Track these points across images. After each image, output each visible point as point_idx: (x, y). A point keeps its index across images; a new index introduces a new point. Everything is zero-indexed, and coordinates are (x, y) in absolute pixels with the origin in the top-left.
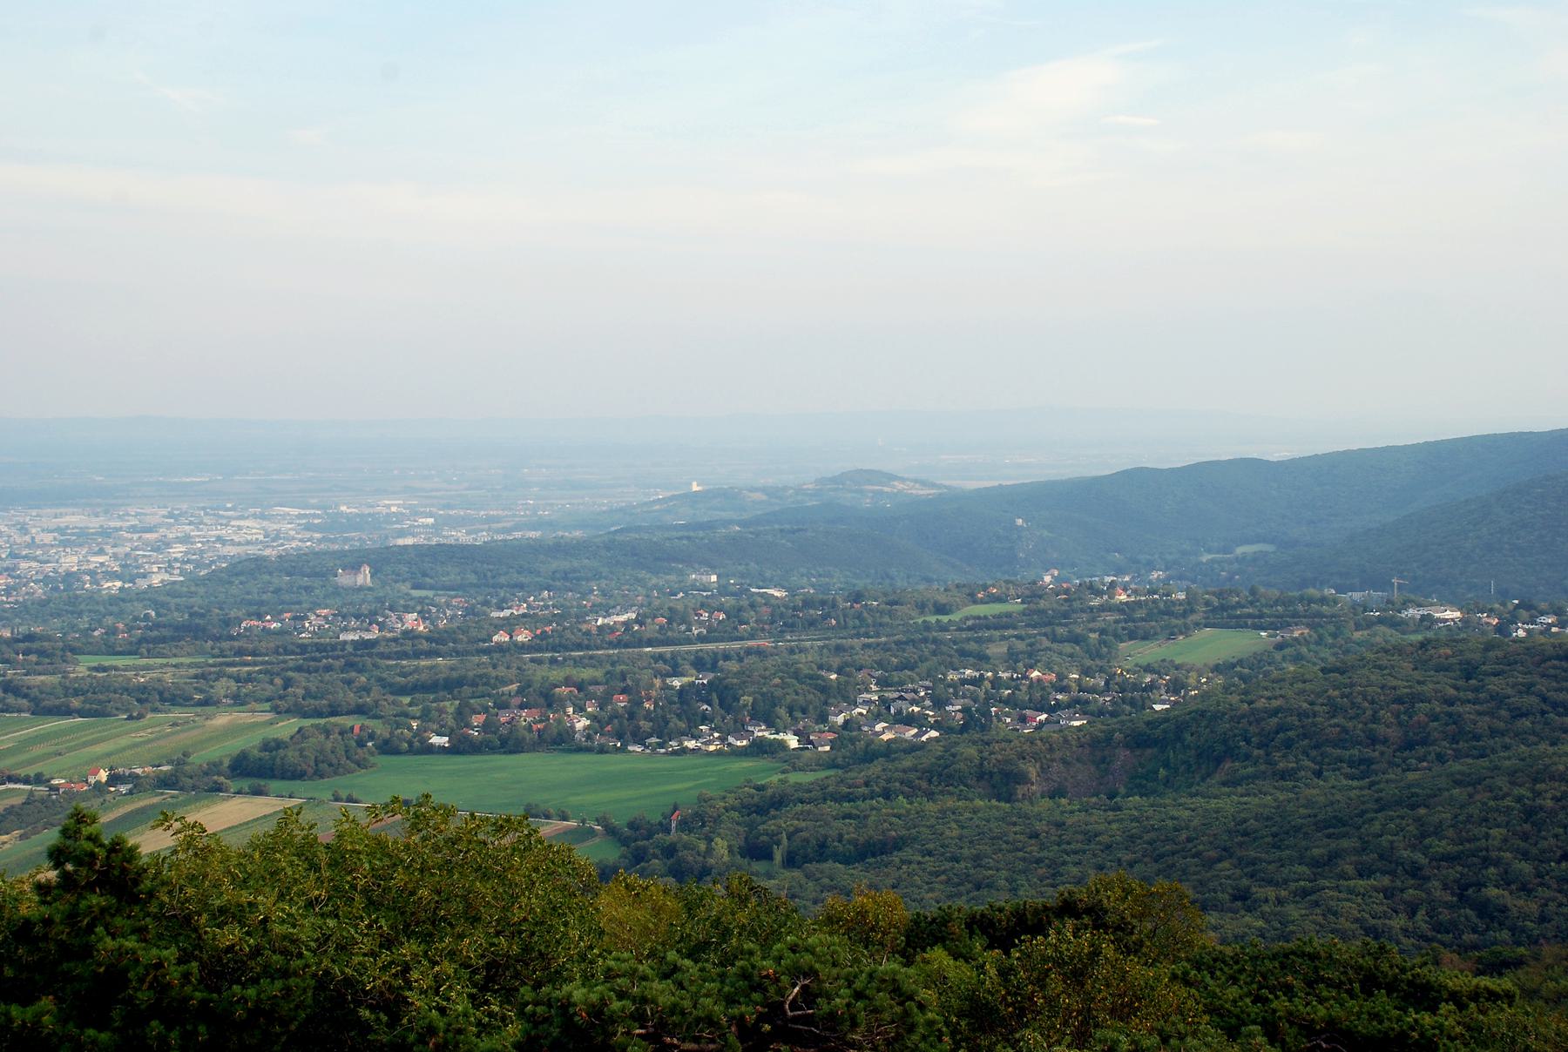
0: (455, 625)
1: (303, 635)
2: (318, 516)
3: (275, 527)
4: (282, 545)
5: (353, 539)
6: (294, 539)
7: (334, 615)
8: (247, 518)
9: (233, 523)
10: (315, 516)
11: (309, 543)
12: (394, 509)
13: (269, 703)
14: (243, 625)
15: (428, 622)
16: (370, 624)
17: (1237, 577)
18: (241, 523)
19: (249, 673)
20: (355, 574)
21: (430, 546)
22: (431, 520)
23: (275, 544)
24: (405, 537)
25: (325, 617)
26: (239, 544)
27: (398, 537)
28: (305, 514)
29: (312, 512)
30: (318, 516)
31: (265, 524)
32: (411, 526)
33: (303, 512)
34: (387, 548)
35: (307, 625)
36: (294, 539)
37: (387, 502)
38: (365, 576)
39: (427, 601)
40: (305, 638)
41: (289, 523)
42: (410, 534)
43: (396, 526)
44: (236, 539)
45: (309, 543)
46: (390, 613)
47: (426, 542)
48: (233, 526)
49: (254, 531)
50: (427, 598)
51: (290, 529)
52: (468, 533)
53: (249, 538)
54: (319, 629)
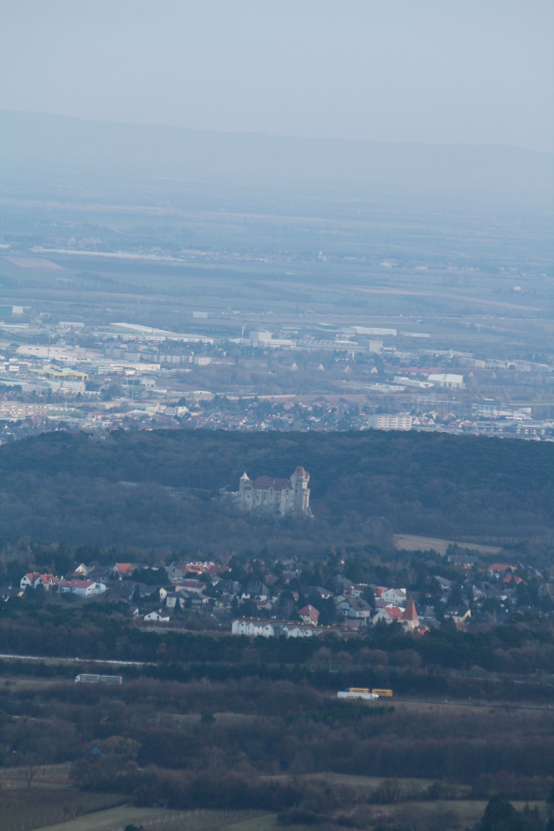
0: (494, 620)
1: (154, 616)
2: (209, 350)
3: (114, 366)
4: (124, 408)
5: (280, 408)
6: (152, 396)
7: (225, 576)
8: (53, 342)
9: (24, 349)
10: (198, 349)
11: (182, 410)
12: (375, 347)
13: (69, 765)
14: (26, 581)
15: (430, 609)
16: (302, 604)
17: (462, 587)
18: (42, 351)
19: (27, 695)
20: (121, 416)
21: (449, 439)
22: (455, 380)
23: (108, 405)
24: (394, 412)
25: (205, 578)
26: (33, 398)
27: (380, 411)
28: (181, 344)
29: (196, 339)
30: (209, 350)
31: (90, 357)
32: (408, 390)
33: (175, 337)
34: (354, 434)
35: (163, 592)
36: (152, 396)
37: (361, 330)
38: (299, 491)
39: (431, 563)
40: (157, 623)
41: (142, 360)
42: (406, 406)
43: (377, 387)
44: (26, 386)
45: (182, 410)
46: (346, 582)
47: (439, 428)
48: (22, 357)
49: (66, 372)
50: (432, 554)
51: (147, 375)
52: (538, 416)
53: (55, 386)
54: (188, 604)
